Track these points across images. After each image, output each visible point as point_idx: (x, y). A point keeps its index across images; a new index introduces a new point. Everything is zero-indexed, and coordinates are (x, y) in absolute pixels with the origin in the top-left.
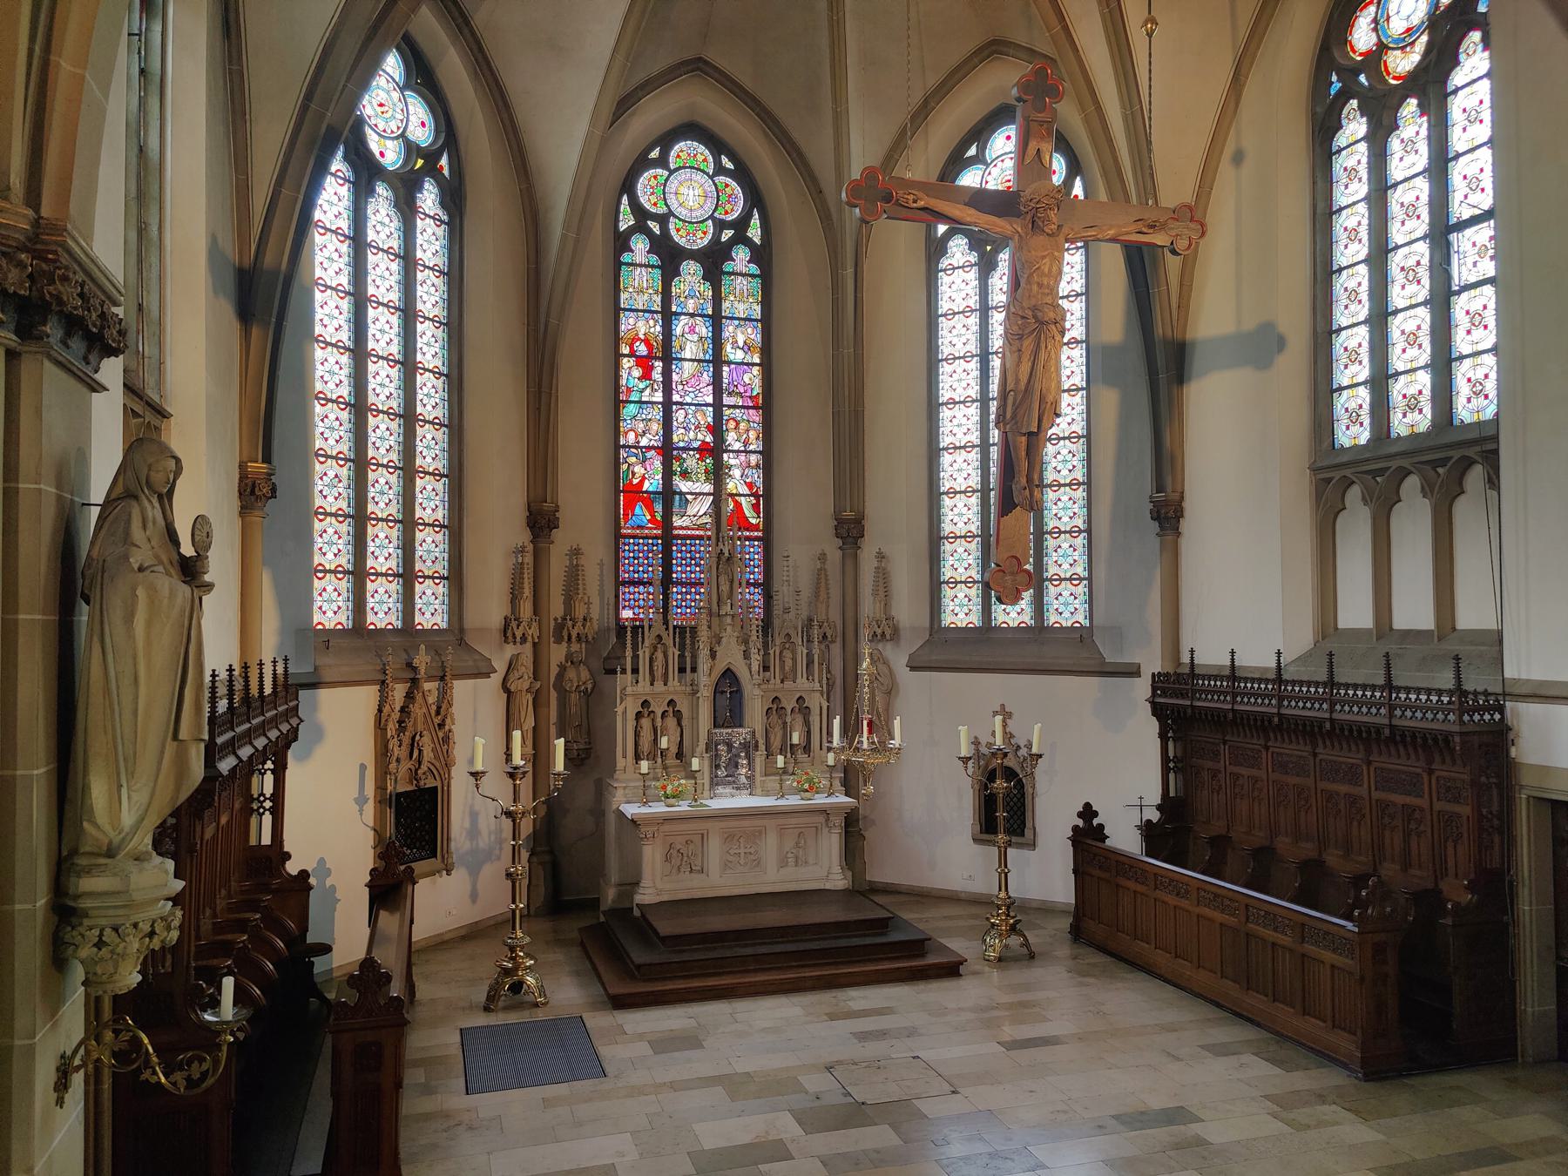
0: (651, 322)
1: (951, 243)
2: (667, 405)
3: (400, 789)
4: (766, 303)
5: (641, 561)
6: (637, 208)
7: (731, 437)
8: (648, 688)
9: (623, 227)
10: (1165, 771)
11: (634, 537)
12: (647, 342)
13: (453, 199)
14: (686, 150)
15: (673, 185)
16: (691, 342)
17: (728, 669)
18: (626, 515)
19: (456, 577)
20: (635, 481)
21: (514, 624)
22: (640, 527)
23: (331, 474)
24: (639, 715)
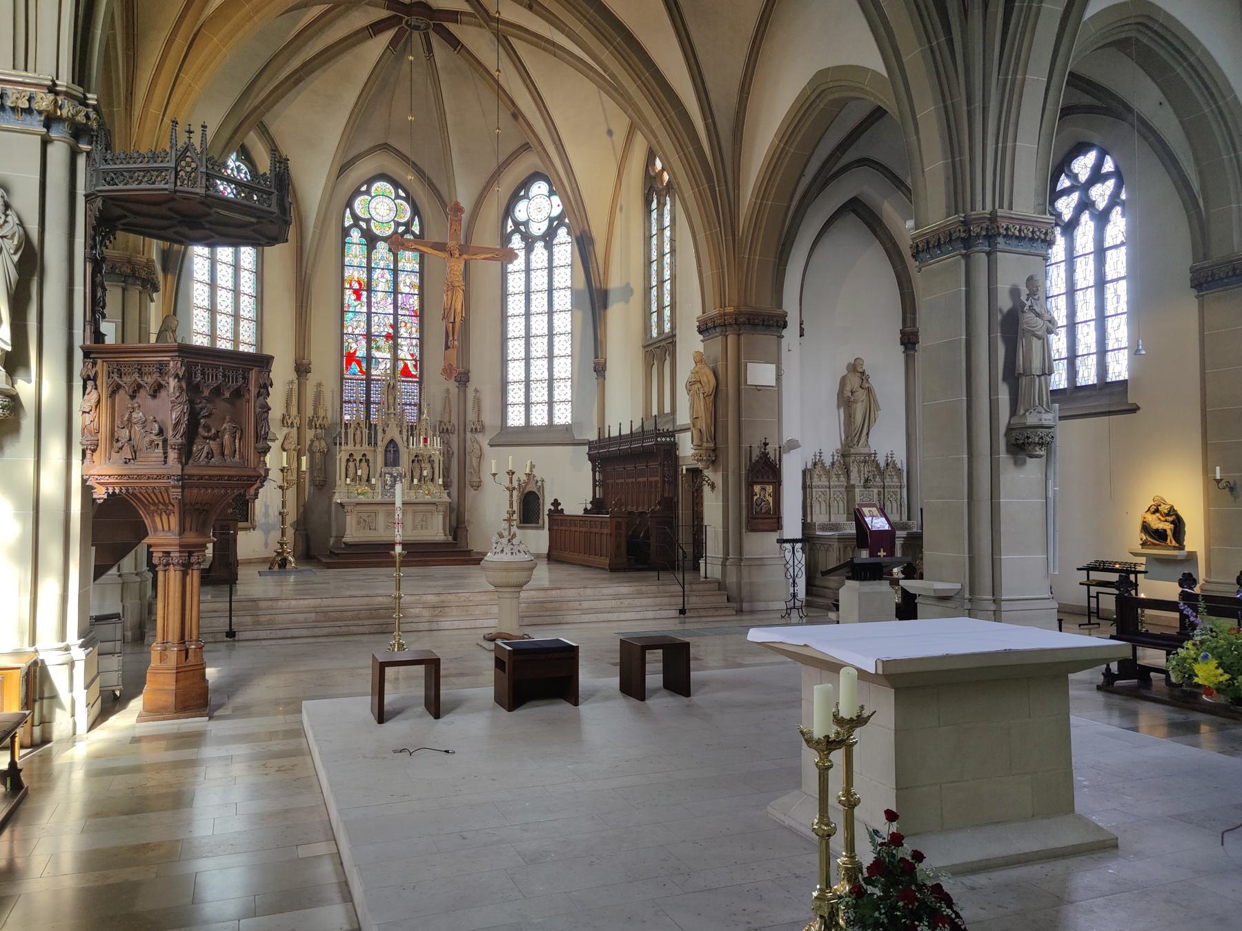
0: (361, 272)
1: (513, 237)
2: (369, 314)
5: (354, 390)
7: (402, 331)
8: (353, 448)
9: (347, 224)
10: (594, 486)
11: (351, 379)
12: (360, 284)
14: (380, 186)
15: (373, 205)
16: (382, 281)
17: (392, 440)
18: (347, 368)
20: (352, 352)
21: (287, 417)
22: (354, 374)
24: (348, 460)
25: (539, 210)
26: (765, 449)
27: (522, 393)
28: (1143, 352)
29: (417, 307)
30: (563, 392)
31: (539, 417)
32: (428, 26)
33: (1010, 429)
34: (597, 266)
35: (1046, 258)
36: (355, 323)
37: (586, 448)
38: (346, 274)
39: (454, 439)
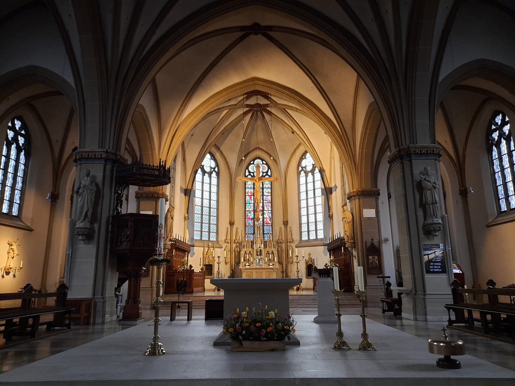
3: (206, 264)
4: (271, 185)
6: (249, 172)
7: (265, 208)
13: (218, 174)
19: (217, 233)
23: (198, 216)
24: (245, 254)
25: (309, 162)
26: (372, 242)
27: (306, 227)
28: (473, 192)
29: (270, 200)
30: (320, 226)
31: (313, 237)
32: (261, 110)
33: (424, 226)
34: (327, 179)
35: (244, 95)
36: (250, 207)
37: (327, 247)
38: (246, 191)
39: (283, 245)
